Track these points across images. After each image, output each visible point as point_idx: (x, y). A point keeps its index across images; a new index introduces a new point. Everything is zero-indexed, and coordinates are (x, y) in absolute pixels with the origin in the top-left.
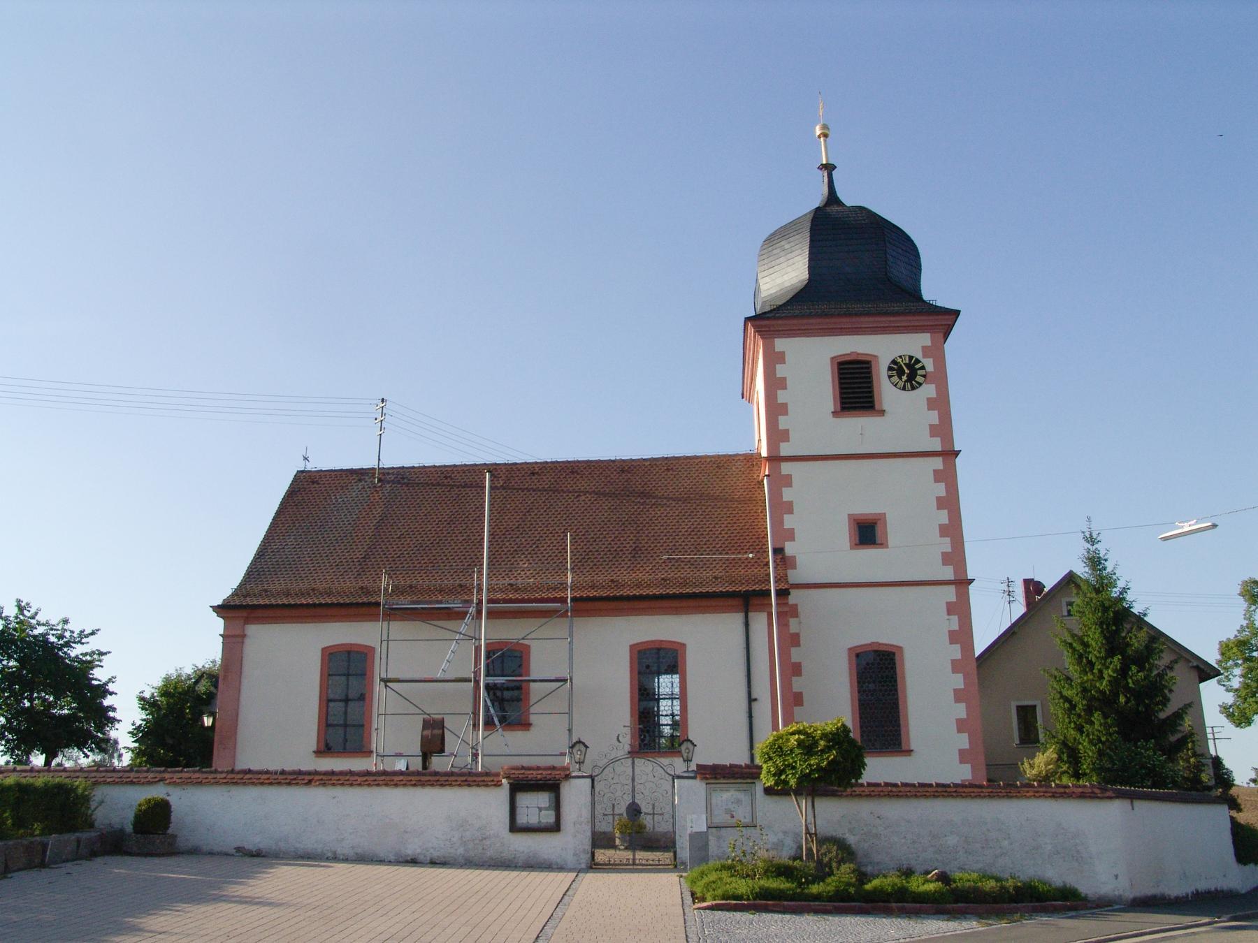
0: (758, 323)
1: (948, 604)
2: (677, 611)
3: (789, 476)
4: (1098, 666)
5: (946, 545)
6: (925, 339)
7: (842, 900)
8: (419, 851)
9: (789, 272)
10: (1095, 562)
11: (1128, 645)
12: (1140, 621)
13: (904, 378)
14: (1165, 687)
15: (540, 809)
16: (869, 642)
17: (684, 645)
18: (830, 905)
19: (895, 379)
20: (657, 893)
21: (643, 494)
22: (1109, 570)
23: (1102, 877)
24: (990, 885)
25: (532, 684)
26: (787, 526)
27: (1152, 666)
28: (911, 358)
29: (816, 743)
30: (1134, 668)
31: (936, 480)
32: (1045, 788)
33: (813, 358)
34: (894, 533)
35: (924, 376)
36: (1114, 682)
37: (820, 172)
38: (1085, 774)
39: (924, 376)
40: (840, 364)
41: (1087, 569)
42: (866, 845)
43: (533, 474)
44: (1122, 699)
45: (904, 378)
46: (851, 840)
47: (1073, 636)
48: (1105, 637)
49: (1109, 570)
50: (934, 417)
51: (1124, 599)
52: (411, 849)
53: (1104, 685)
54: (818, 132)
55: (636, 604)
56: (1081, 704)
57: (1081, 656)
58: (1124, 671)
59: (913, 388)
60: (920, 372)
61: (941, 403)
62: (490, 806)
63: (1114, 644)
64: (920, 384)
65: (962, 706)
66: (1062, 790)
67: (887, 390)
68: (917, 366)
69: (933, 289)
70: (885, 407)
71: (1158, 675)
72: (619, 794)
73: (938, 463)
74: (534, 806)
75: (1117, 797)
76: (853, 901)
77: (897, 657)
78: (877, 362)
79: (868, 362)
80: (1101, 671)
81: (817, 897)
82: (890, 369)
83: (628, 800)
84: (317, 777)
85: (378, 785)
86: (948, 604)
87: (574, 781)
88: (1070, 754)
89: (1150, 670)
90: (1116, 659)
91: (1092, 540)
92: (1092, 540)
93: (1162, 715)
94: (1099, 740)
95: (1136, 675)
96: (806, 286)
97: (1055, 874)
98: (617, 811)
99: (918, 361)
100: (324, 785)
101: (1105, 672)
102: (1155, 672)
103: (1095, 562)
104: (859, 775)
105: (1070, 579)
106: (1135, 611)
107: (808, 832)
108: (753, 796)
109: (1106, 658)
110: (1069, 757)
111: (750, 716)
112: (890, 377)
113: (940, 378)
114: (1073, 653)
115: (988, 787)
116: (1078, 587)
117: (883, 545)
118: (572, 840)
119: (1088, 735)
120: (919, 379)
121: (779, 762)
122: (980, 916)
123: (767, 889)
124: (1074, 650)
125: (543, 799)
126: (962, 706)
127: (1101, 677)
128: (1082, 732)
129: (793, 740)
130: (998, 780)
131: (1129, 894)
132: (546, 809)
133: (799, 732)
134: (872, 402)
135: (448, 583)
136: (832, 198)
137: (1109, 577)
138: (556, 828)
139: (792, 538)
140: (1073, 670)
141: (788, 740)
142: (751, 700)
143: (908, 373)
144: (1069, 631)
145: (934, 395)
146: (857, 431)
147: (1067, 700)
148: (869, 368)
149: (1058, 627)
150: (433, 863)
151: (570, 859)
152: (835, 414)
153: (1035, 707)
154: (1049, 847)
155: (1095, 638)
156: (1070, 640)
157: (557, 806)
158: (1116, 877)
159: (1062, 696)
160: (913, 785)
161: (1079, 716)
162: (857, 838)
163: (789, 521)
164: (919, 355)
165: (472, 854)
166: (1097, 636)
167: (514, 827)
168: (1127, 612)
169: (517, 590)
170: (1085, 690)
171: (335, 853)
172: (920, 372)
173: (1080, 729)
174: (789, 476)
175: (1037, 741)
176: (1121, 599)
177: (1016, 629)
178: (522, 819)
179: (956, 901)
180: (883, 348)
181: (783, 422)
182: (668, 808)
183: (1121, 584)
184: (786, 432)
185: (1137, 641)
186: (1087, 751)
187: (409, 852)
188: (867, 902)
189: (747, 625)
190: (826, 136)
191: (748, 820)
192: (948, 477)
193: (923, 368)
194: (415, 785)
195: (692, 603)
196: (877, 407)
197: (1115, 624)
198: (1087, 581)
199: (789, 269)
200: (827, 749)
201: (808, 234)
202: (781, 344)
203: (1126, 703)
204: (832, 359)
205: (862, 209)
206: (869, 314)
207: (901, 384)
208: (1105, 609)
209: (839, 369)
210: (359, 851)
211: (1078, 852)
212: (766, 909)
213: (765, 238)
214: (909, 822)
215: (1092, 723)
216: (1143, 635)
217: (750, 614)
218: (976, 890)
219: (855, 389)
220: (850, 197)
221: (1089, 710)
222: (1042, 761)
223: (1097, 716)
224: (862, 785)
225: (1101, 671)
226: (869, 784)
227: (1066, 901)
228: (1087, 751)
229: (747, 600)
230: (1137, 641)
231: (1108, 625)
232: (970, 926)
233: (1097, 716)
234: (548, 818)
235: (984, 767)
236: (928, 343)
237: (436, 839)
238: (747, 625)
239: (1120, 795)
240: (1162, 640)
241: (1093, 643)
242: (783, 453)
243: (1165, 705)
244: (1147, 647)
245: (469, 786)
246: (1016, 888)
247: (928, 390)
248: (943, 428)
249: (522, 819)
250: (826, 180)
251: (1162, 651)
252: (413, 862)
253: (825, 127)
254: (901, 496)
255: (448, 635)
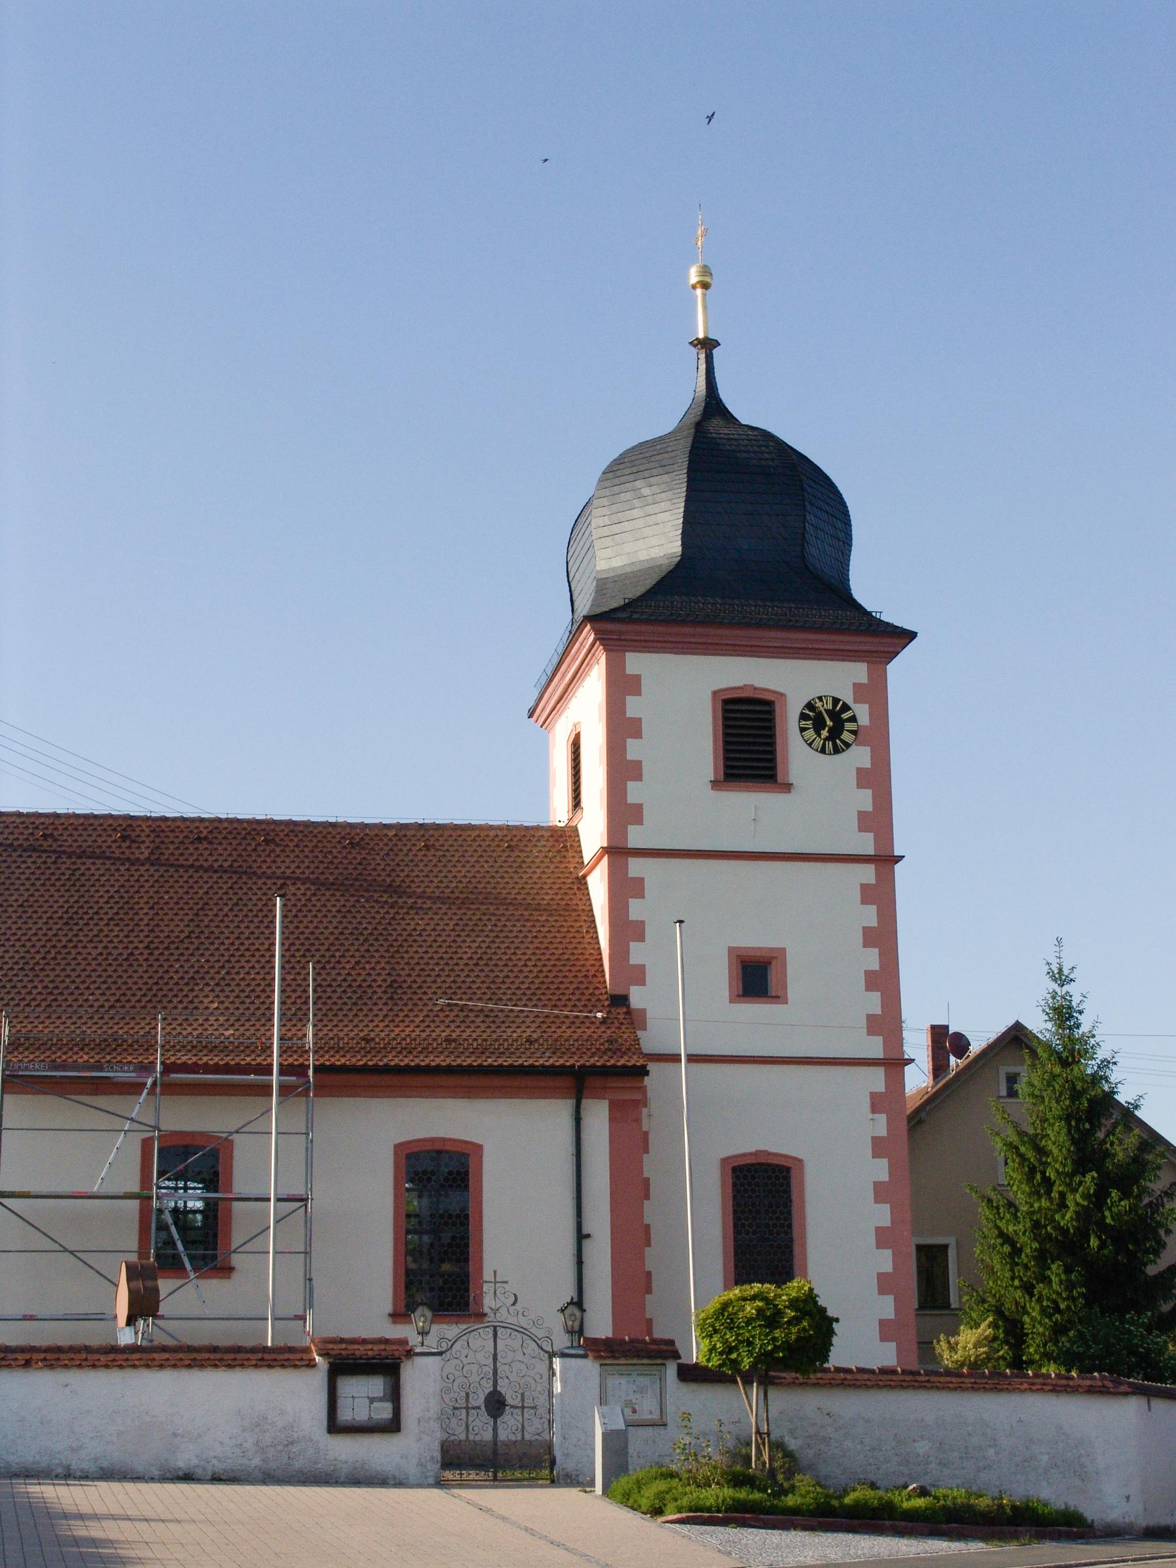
0: (600, 626)
1: (873, 1095)
2: (469, 1093)
3: (640, 881)
4: (1058, 1188)
5: (873, 1003)
6: (859, 671)
7: (823, 1515)
8: (195, 1461)
9: (650, 534)
10: (1064, 1014)
11: (1107, 1154)
12: (1128, 1116)
13: (825, 733)
14: (1160, 1225)
15: (372, 1400)
16: (752, 1149)
17: (478, 1148)
18: (814, 1521)
19: (810, 734)
20: (579, 1514)
21: (390, 889)
22: (1084, 1029)
23: (1109, 1501)
24: (983, 1503)
25: (235, 1204)
26: (633, 960)
27: (1144, 1191)
28: (836, 701)
29: (779, 1313)
30: (1115, 1194)
31: (864, 901)
32: (975, 1377)
33: (688, 687)
34: (798, 978)
35: (854, 732)
36: (1083, 1215)
37: (694, 350)
38: (1031, 1362)
39: (854, 732)
40: (726, 702)
41: (1049, 1025)
42: (811, 1452)
43: (200, 839)
44: (1094, 1242)
45: (825, 733)
46: (792, 1444)
47: (1021, 1134)
48: (1074, 1142)
49: (1084, 1029)
50: (865, 800)
51: (1106, 1079)
52: (185, 1459)
53: (1067, 1219)
54: (694, 278)
55: (407, 1080)
56: (1030, 1246)
57: (1032, 1171)
58: (1099, 1198)
59: (837, 751)
60: (848, 726)
61: (877, 778)
62: (298, 1397)
63: (1086, 1155)
64: (848, 745)
65: (887, 1254)
66: (1064, 1382)
67: (797, 752)
68: (845, 716)
69: (872, 583)
70: (792, 779)
71: (1150, 1204)
72: (475, 1378)
73: (867, 873)
74: (362, 1396)
75: (1133, 1393)
76: (836, 1516)
77: (793, 1173)
78: (784, 704)
79: (770, 703)
80: (1062, 1195)
81: (795, 1511)
82: (803, 717)
83: (489, 1387)
84: (36, 1356)
85: (134, 1366)
86: (873, 1095)
87: (419, 1360)
88: (1011, 1330)
89: (1139, 1197)
90: (1088, 1178)
91: (1061, 977)
92: (1061, 977)
93: (1152, 1270)
94: (1057, 1310)
95: (1118, 1204)
96: (678, 565)
97: (1053, 1494)
98: (472, 1403)
99: (846, 708)
100: (51, 1367)
101: (1070, 1198)
102: (1146, 1201)
103: (1064, 1014)
104: (826, 1358)
105: (1016, 1038)
106: (1122, 1098)
107: (758, 1432)
108: (662, 1379)
109: (1071, 1175)
110: (1006, 1333)
111: (580, 1262)
112: (802, 730)
113: (878, 738)
114: (1021, 1164)
115: (970, 1375)
116: (1033, 1053)
117: (780, 998)
118: (416, 1444)
119: (1039, 1300)
120: (846, 736)
121: (730, 1337)
122: (985, 1538)
123: (739, 1501)
124: (1022, 1156)
125: (376, 1385)
126: (887, 1254)
127: (1063, 1205)
128: (1031, 1295)
129: (750, 1309)
130: (921, 1374)
131: (1142, 1522)
132: (381, 1400)
133: (754, 1298)
134: (774, 768)
135: (92, 1031)
136: (713, 405)
137: (1083, 1040)
138: (393, 1426)
139: (642, 981)
140: (1020, 1193)
141: (742, 1309)
142: (581, 1237)
143: (830, 725)
144: (1016, 1126)
145: (867, 763)
146: (747, 814)
147: (1006, 1239)
148: (771, 712)
149: (998, 1119)
150: (216, 1479)
151: (412, 1470)
152: (715, 784)
153: (945, 1247)
154: (1045, 1458)
155: (1057, 1140)
156: (1014, 1138)
157: (395, 1395)
158: (1128, 1498)
159: (1001, 1234)
160: (872, 1372)
161: (1026, 1267)
162: (800, 1442)
163: (638, 953)
164: (847, 697)
165: (273, 1465)
166: (1063, 1137)
167: (335, 1427)
168: (1108, 1099)
169: (213, 1049)
170: (1036, 1225)
171: (68, 1467)
172: (848, 726)
173: (1028, 1289)
174: (640, 881)
175: (947, 1305)
176: (1096, 1079)
177: (923, 1115)
178: (345, 1415)
179: (948, 1521)
180: (797, 681)
181: (635, 792)
182: (542, 1400)
183: (1101, 1054)
184: (639, 808)
185: (1122, 1149)
186: (1035, 1323)
187: (181, 1464)
188: (851, 1518)
189: (578, 1120)
190: (705, 286)
191: (656, 1416)
192: (881, 896)
193: (853, 719)
194: (189, 1366)
195: (497, 1081)
196: (780, 778)
197: (1089, 1120)
198: (1048, 1046)
199: (648, 531)
200: (795, 1321)
201: (684, 477)
202: (635, 662)
203: (1100, 1248)
204: (715, 693)
205: (767, 437)
206: (777, 627)
207: (819, 743)
208: (1076, 1095)
209: (725, 711)
210: (105, 1464)
211: (1082, 1466)
212: (743, 1524)
213: (604, 466)
214: (868, 1421)
215: (1046, 1280)
216: (1132, 1140)
217: (584, 1101)
218: (969, 1508)
219: (748, 745)
220: (748, 407)
221: (1042, 1257)
222: (968, 1341)
223: (1056, 1270)
224: (827, 1370)
225: (1062, 1195)
226: (838, 1370)
227: (1068, 1526)
228: (1035, 1323)
229: (576, 1082)
230: (1122, 1149)
231: (1079, 1120)
232: (975, 1547)
233: (1056, 1270)
234: (384, 1411)
235: (915, 1347)
236: (863, 679)
237: (221, 1442)
238: (578, 1120)
239: (1138, 1391)
240: (1159, 1149)
241: (1055, 1151)
242: (632, 844)
243: (1157, 1253)
244: (1136, 1160)
245: (269, 1366)
246: (1014, 1508)
247: (859, 756)
248: (878, 819)
249: (345, 1415)
250: (703, 367)
251: (1159, 1168)
252: (187, 1477)
253: (705, 271)
254: (812, 923)
255: (106, 1121)
